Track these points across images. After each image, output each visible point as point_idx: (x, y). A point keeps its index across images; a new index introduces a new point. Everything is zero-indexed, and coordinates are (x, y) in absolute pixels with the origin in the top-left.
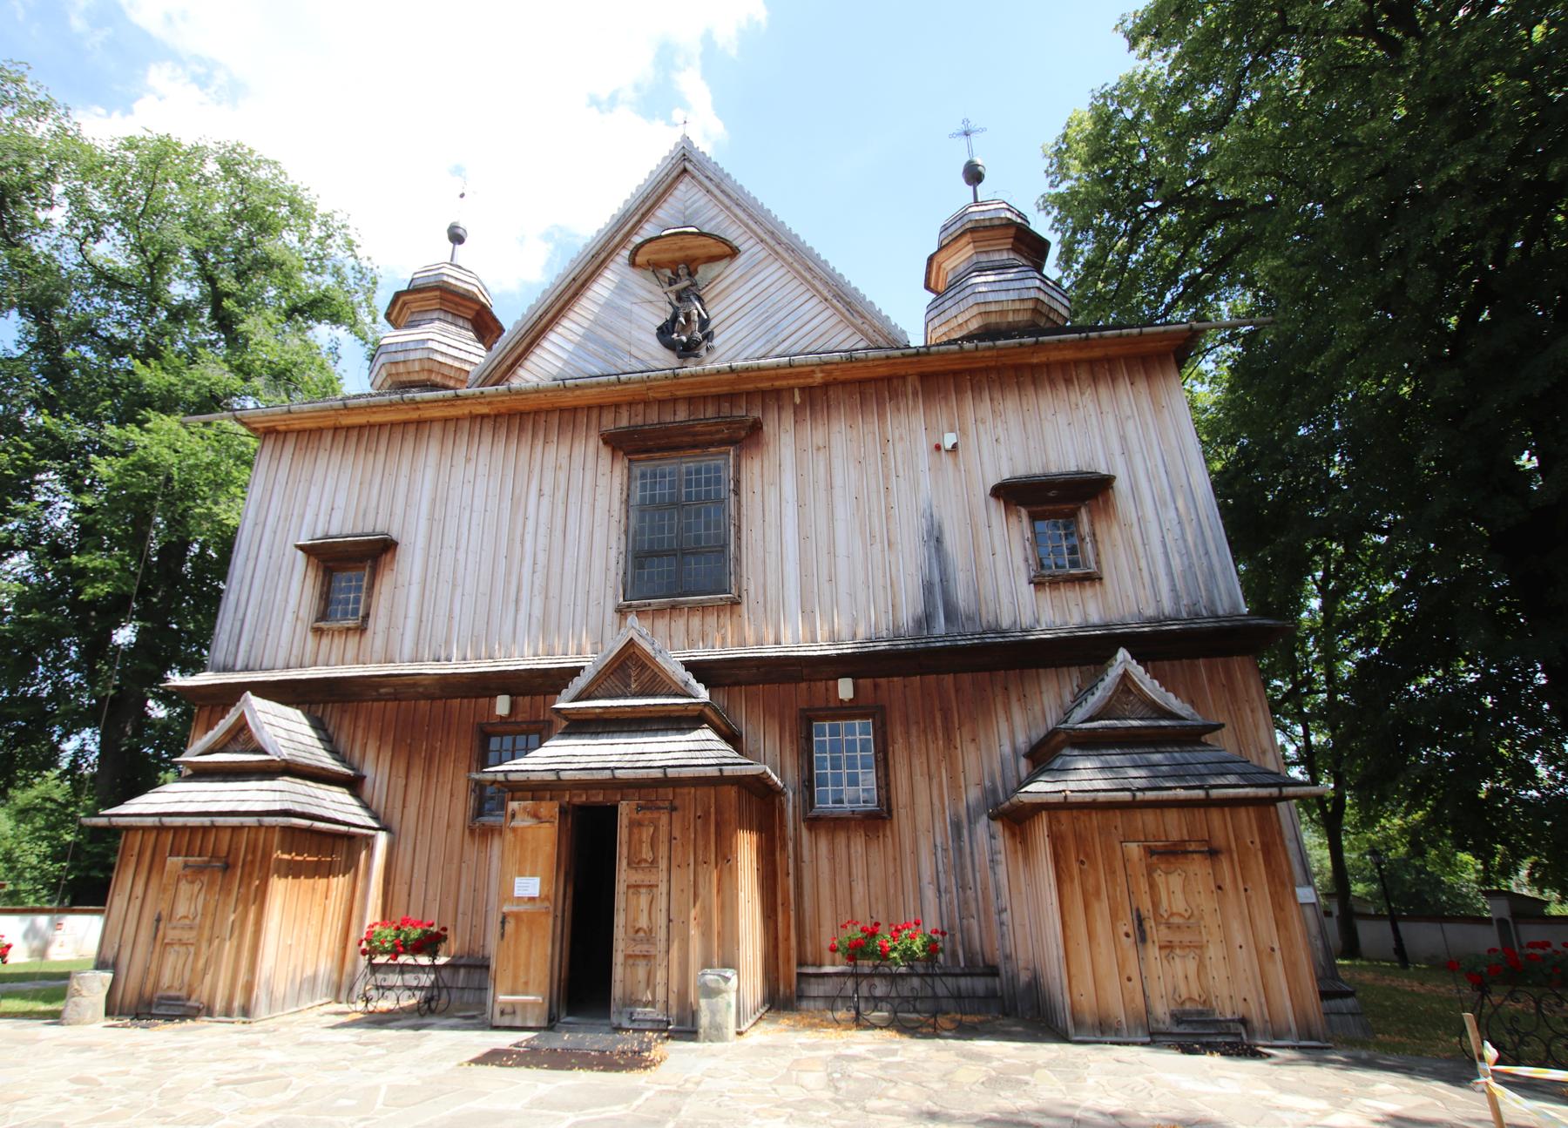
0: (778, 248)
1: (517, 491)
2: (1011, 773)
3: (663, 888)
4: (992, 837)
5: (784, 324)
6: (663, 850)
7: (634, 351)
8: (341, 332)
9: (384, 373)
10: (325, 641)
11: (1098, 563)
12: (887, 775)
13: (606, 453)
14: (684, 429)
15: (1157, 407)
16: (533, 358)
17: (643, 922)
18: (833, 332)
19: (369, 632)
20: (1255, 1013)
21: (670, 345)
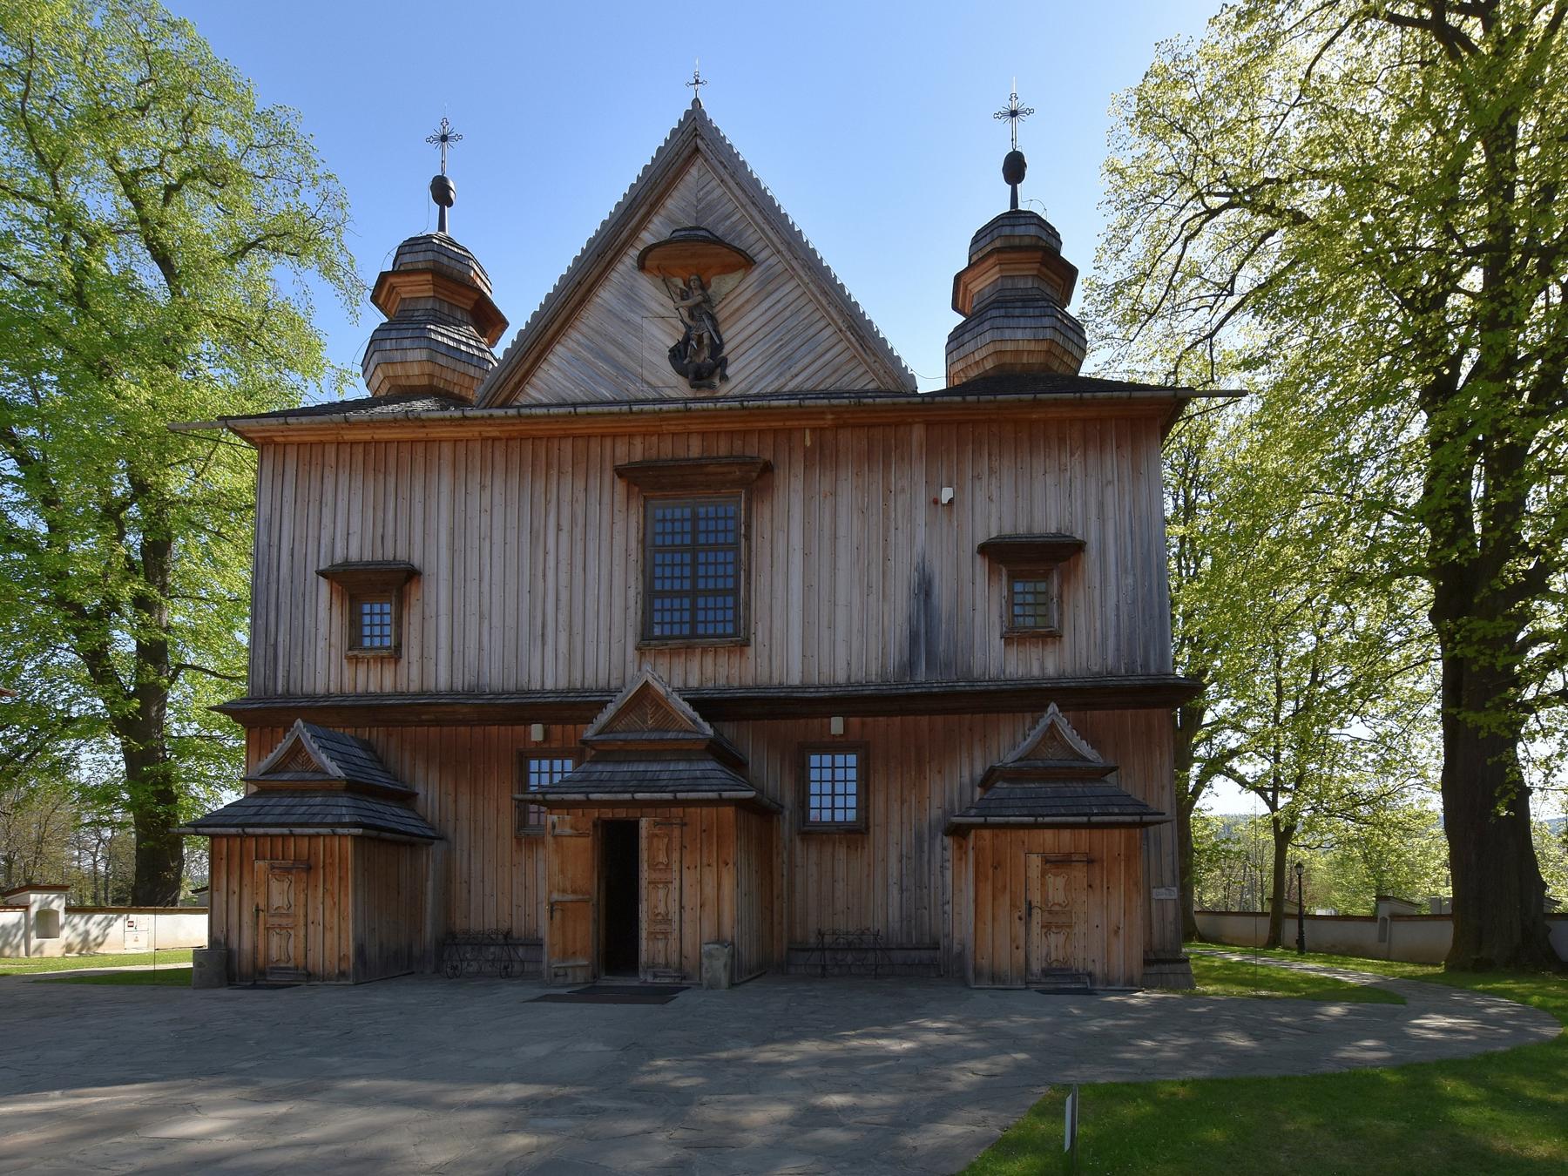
0: (794, 263)
1: (535, 524)
2: (967, 797)
3: (676, 883)
4: (944, 849)
5: (798, 355)
6: (676, 856)
7: (646, 374)
8: (311, 274)
9: (380, 374)
10: (362, 668)
11: (1061, 621)
12: (867, 799)
13: (620, 487)
14: (698, 465)
15: (1136, 470)
16: (540, 373)
17: (661, 909)
18: (847, 368)
19: (404, 661)
20: (1097, 969)
21: (682, 371)
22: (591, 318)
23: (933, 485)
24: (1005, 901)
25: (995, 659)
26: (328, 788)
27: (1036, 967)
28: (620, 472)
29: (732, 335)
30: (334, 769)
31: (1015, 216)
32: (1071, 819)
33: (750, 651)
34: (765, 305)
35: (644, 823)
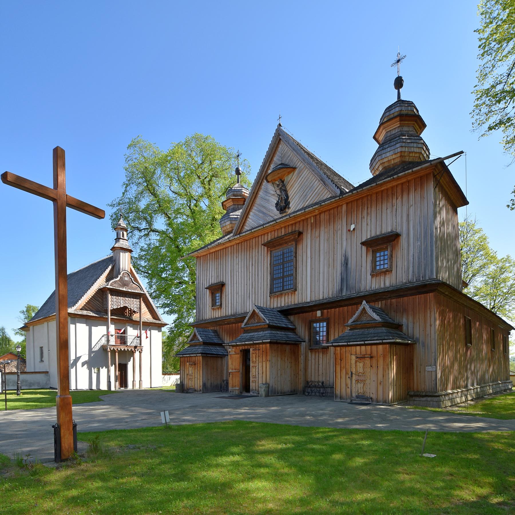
5: (308, 194)
6: (257, 359)
15: (422, 197)
16: (247, 222)
20: (374, 396)
22: (258, 201)
23: (348, 224)
24: (344, 371)
25: (369, 283)
26: (375, 325)
27: (354, 395)
28: (264, 245)
29: (291, 193)
30: (201, 340)
31: (400, 102)
32: (375, 342)
33: (297, 292)
34: (299, 180)
35: (251, 350)
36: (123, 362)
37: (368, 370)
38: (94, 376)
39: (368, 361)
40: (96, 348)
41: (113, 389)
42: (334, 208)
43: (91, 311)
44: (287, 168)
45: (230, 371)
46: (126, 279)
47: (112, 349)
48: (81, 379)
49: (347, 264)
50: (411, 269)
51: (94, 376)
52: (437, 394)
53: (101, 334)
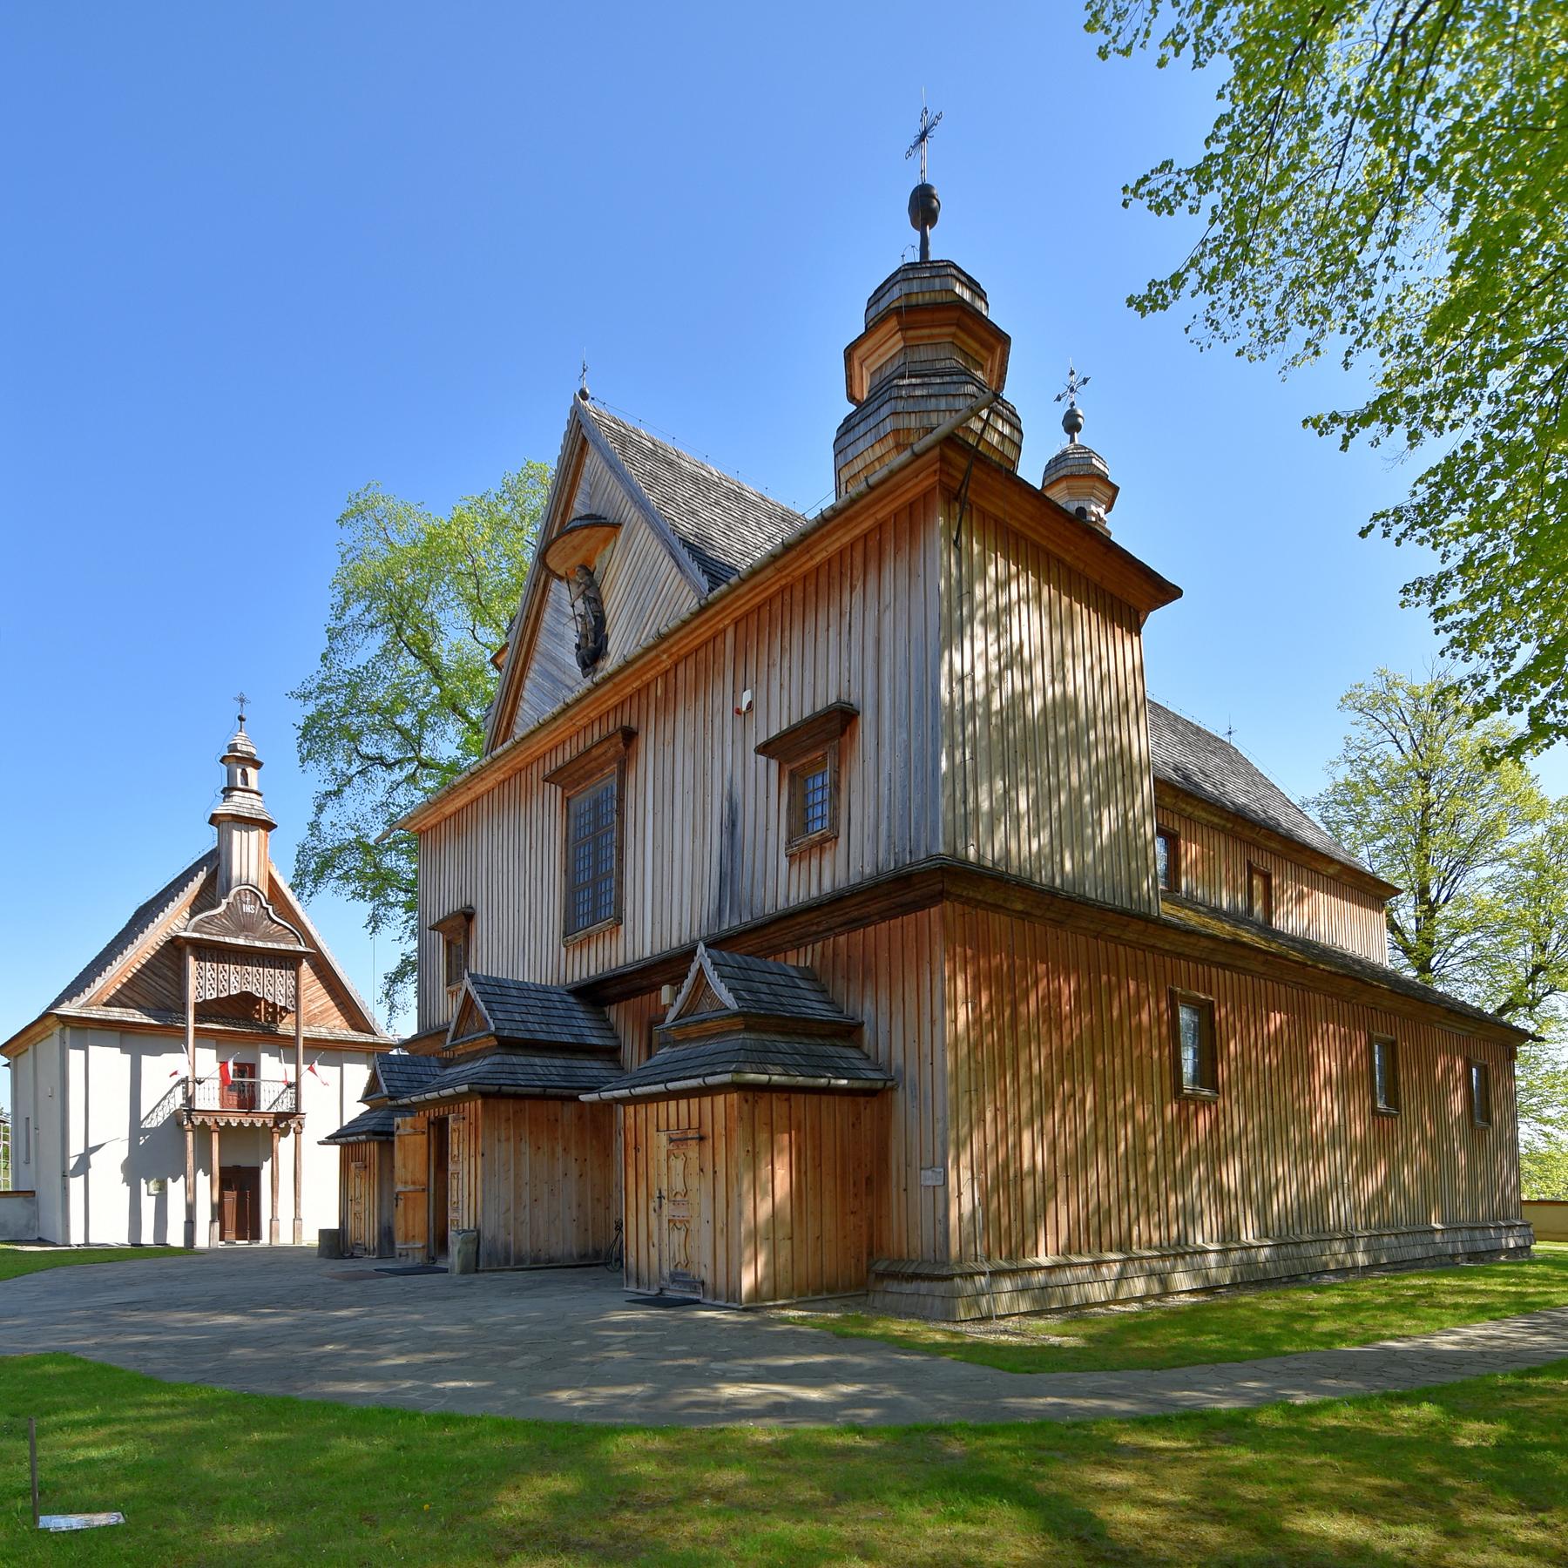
16: (520, 712)
27: (666, 1272)
29: (610, 608)
31: (924, 267)
36: (245, 1162)
37: (694, 1182)
38: (148, 1205)
39: (693, 1150)
40: (156, 1121)
41: (202, 1241)
42: (706, 643)
43: (139, 1008)
44: (603, 525)
45: (399, 1188)
46: (248, 909)
47: (197, 1123)
48: (101, 1212)
49: (733, 824)
50: (884, 826)
51: (148, 1205)
52: (945, 1272)
53: (190, 1073)
